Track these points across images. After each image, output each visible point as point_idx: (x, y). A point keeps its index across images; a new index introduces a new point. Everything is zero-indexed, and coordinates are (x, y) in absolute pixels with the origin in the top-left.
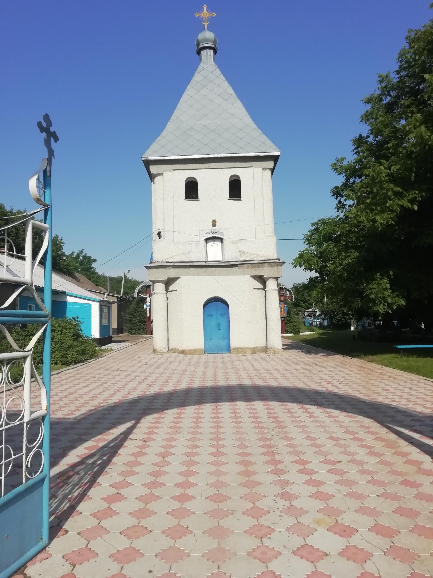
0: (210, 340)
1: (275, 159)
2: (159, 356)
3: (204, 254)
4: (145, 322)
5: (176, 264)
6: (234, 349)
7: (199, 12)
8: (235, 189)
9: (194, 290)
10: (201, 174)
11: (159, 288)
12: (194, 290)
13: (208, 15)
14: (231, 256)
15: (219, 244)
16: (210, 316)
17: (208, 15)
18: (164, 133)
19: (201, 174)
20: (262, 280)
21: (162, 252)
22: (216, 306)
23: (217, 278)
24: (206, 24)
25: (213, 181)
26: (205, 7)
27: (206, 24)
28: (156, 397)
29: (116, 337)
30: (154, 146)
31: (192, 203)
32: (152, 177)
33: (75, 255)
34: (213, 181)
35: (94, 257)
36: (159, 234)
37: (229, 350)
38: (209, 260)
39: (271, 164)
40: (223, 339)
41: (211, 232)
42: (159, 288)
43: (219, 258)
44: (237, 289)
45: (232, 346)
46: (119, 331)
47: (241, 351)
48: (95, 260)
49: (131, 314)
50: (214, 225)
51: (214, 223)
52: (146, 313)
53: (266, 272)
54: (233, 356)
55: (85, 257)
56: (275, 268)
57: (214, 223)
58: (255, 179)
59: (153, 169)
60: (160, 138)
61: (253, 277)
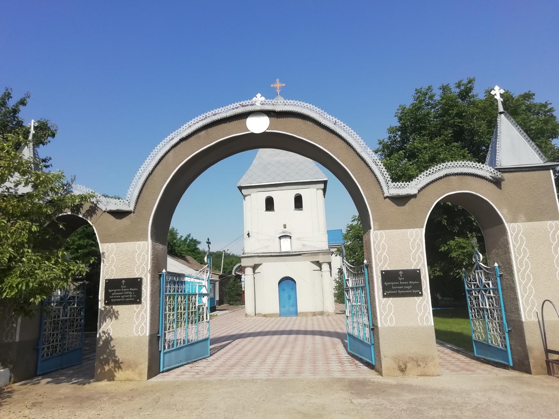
0: (284, 307)
1: (325, 183)
2: (248, 319)
3: (279, 247)
4: (241, 295)
5: (260, 255)
6: (300, 313)
7: (274, 83)
8: (298, 202)
9: (271, 272)
10: (275, 194)
11: (249, 271)
12: (271, 272)
13: (280, 85)
14: (297, 248)
15: (289, 240)
16: (284, 290)
17: (280, 85)
18: (251, 167)
19: (275, 194)
20: (318, 264)
21: (251, 246)
22: (287, 283)
23: (287, 263)
24: (278, 91)
25: (284, 198)
26: (278, 80)
27: (278, 91)
28: (243, 334)
29: (218, 307)
30: (245, 177)
31: (270, 213)
32: (245, 196)
33: (183, 239)
34: (284, 198)
35: (198, 240)
36: (248, 234)
37: (296, 313)
38: (282, 251)
39: (322, 186)
40: (293, 306)
41: (283, 232)
42: (249, 271)
43: (289, 249)
44: (300, 270)
45: (299, 311)
46: (221, 302)
47: (305, 314)
48: (199, 243)
49: (230, 288)
50: (285, 228)
51: (285, 226)
52: (242, 287)
53: (321, 258)
54: (299, 318)
55: (192, 240)
56: (327, 256)
57: (285, 226)
58: (311, 195)
59: (244, 192)
60: (248, 171)
61: (312, 262)
